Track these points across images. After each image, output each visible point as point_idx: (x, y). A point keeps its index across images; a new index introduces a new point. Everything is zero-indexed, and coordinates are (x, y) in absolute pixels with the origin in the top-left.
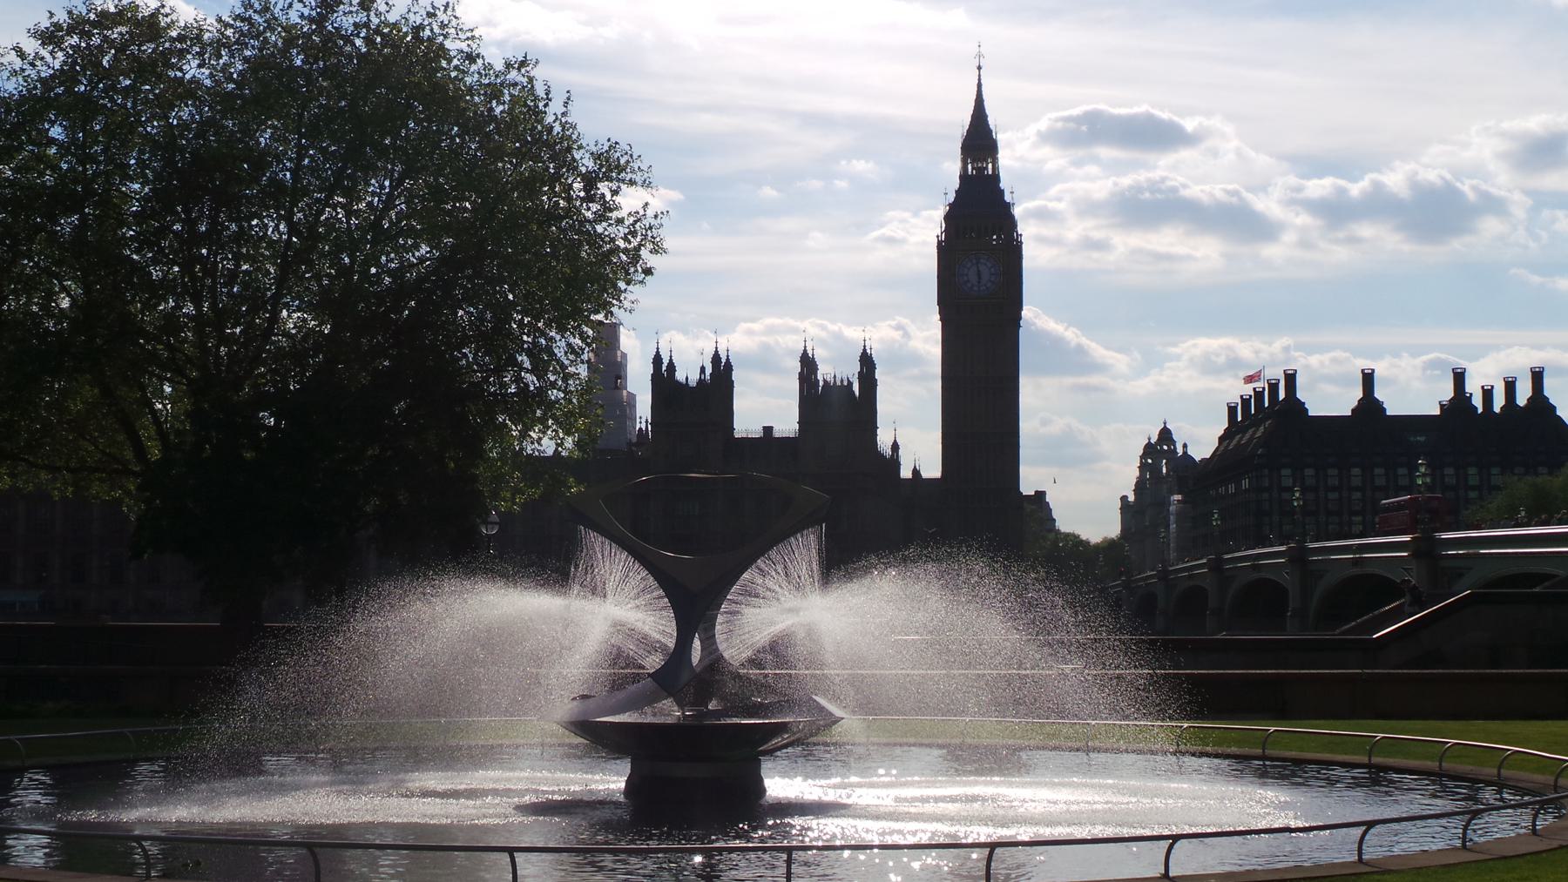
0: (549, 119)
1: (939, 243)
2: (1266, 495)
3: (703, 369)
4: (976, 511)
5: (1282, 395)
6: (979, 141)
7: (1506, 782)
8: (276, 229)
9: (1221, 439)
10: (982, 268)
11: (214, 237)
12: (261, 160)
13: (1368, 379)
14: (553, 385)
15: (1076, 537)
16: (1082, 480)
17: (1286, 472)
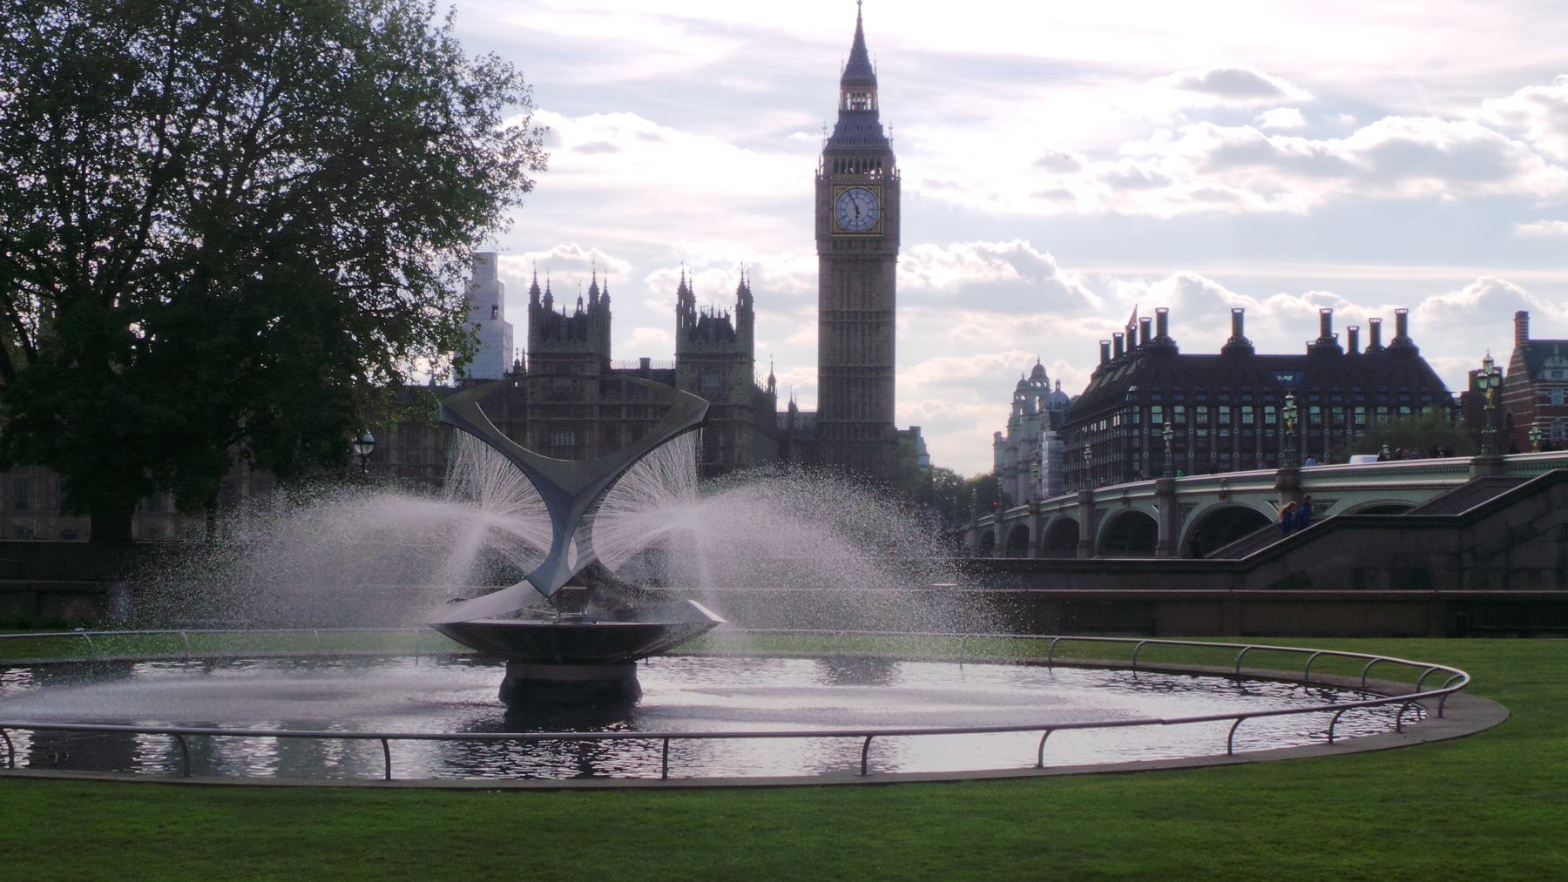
0: (429, 33)
1: (818, 177)
2: (1136, 433)
3: (580, 301)
4: (853, 434)
5: (1153, 334)
6: (859, 76)
7: (1370, 689)
8: (146, 142)
9: (1094, 377)
10: (858, 202)
11: (83, 147)
12: (133, 70)
14: (429, 302)
15: (950, 472)
16: (954, 404)
17: (1156, 409)
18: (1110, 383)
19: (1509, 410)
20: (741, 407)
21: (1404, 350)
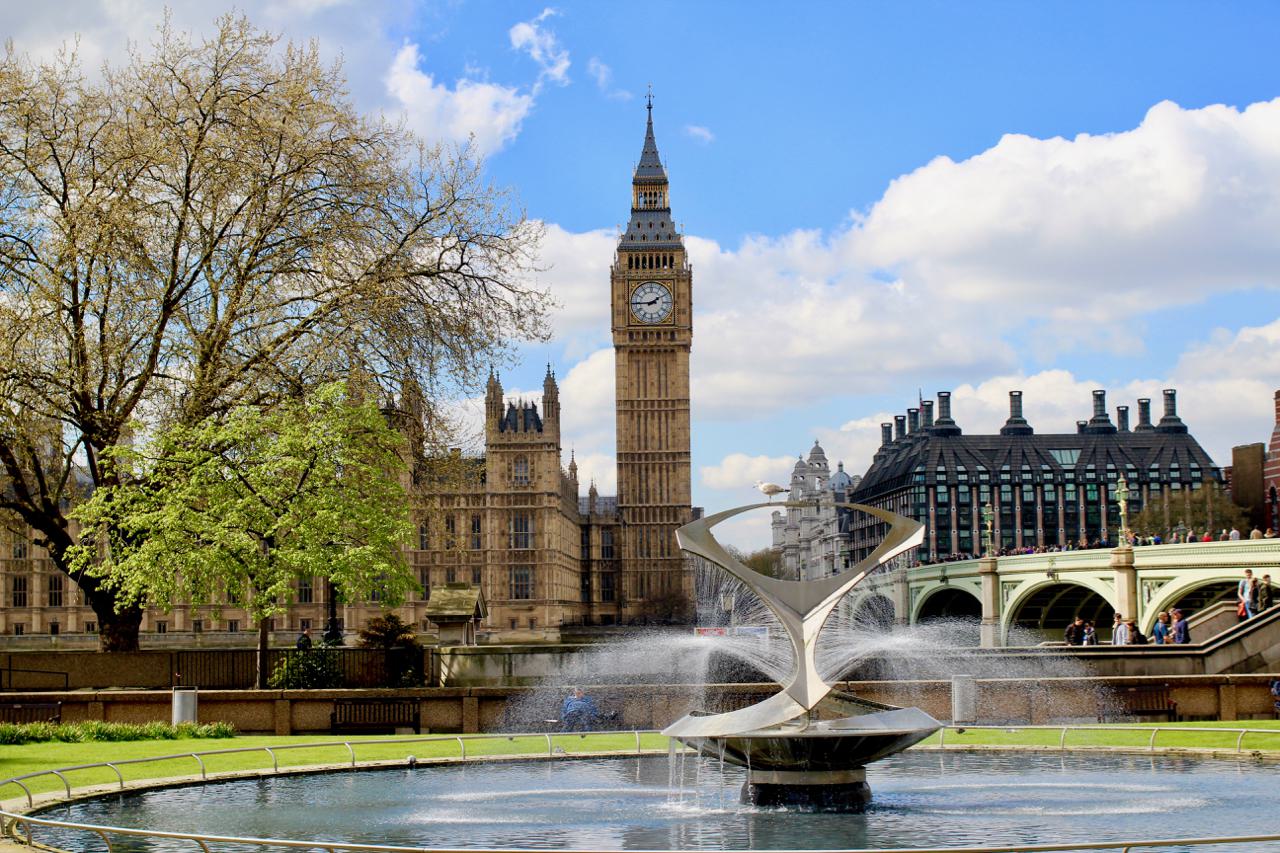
5: (936, 416)
9: (877, 458)
13: (1016, 399)
18: (895, 463)
19: (1272, 484)
20: (550, 494)
21: (1174, 429)
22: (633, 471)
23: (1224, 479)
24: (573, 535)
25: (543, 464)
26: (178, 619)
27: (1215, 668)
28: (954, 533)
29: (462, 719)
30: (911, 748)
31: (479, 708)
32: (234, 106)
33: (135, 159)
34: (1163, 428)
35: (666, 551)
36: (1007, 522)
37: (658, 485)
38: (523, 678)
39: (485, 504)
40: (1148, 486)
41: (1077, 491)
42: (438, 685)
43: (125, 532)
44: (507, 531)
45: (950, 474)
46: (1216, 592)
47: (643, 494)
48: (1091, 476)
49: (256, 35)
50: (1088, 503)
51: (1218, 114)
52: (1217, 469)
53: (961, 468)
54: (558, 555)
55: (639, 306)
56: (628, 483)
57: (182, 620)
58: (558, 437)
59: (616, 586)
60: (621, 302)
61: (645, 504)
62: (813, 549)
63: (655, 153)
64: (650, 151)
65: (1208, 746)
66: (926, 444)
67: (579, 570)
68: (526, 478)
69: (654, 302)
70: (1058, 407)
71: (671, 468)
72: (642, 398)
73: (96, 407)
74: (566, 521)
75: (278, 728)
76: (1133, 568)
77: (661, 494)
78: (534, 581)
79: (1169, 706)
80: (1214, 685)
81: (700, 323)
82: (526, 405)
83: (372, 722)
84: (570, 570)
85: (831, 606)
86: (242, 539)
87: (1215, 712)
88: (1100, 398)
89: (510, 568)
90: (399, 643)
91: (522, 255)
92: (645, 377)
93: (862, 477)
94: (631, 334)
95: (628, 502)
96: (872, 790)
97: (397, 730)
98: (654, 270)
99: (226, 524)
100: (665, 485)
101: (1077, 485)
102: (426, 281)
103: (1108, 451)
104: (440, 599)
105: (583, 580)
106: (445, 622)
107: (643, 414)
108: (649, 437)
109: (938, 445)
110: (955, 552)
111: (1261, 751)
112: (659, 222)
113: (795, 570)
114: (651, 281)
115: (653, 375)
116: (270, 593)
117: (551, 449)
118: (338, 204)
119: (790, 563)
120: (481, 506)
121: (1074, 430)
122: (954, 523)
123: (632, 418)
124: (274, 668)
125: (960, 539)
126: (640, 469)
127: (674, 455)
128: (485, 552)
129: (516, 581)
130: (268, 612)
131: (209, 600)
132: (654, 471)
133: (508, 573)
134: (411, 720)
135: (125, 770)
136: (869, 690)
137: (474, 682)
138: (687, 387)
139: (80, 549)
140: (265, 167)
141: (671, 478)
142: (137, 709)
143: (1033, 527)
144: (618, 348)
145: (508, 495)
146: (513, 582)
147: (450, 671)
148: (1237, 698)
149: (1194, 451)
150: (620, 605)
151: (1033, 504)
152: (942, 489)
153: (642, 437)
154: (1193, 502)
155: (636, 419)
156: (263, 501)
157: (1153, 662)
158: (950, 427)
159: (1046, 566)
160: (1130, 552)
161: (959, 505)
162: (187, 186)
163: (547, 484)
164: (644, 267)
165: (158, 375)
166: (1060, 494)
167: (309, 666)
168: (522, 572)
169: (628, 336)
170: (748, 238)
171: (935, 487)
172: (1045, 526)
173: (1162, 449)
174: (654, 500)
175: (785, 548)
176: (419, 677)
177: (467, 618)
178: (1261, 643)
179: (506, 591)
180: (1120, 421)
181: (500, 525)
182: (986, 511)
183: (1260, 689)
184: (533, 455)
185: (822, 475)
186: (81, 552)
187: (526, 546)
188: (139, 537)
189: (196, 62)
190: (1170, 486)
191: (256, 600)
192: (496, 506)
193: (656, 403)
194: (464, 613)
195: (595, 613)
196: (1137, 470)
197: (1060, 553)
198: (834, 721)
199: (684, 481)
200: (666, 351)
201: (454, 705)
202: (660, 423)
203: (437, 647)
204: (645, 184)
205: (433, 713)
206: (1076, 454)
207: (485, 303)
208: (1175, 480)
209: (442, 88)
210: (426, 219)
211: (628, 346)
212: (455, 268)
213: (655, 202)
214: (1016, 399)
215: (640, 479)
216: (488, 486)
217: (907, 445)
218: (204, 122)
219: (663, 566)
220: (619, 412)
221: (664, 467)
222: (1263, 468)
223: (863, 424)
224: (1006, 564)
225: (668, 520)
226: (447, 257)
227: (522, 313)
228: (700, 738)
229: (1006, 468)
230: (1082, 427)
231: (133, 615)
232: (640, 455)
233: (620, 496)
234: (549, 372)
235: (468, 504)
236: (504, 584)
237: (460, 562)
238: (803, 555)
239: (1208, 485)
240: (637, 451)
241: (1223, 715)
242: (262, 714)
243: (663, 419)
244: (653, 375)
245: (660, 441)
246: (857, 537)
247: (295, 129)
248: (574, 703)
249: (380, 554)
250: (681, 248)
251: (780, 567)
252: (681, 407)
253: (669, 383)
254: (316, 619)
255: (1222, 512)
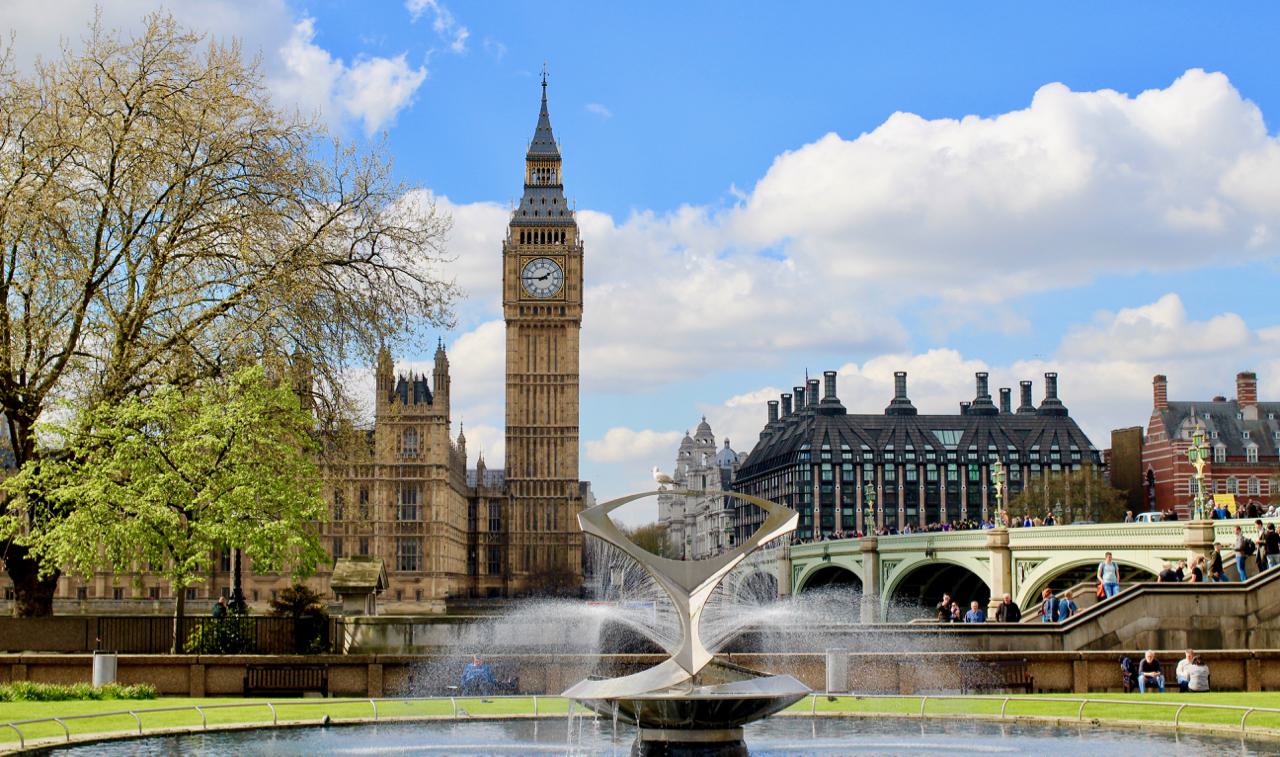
5: (822, 395)
9: (763, 435)
13: (901, 379)
18: (781, 441)
19: (1150, 467)
20: (439, 467)
21: (1055, 412)
22: (521, 445)
23: (1103, 461)
24: (460, 507)
25: (433, 436)
26: (99, 586)
27: (1074, 645)
28: (838, 512)
29: (366, 685)
30: (779, 713)
31: (384, 674)
32: (160, 100)
33: (62, 146)
34: (1044, 410)
35: (552, 525)
36: (890, 501)
37: (546, 459)
38: (423, 647)
39: (373, 475)
40: (1029, 467)
41: (959, 471)
42: (342, 653)
43: (52, 504)
44: (395, 503)
45: (834, 452)
46: (1088, 573)
47: (531, 468)
48: (973, 456)
49: (181, 33)
50: (970, 483)
51: (1109, 98)
52: (1097, 452)
53: (845, 447)
54: (445, 527)
55: (530, 281)
56: (515, 456)
57: (67, 587)
58: (448, 409)
59: (502, 559)
60: (513, 277)
61: (532, 478)
62: (698, 525)
63: (549, 130)
64: (544, 129)
65: (1054, 715)
66: (812, 422)
67: (466, 542)
68: (415, 450)
69: (545, 278)
70: (941, 386)
71: (559, 442)
72: (531, 372)
73: (18, 382)
74: (453, 493)
75: (192, 691)
76: (1008, 548)
77: (549, 467)
78: (421, 552)
79: (1026, 679)
80: (1070, 660)
81: (589, 295)
82: (416, 377)
83: (273, 686)
84: (457, 542)
85: (715, 583)
86: (162, 512)
87: (1069, 686)
88: (982, 379)
89: (397, 539)
90: (308, 612)
91: (430, 247)
92: (535, 352)
93: (749, 454)
94: (522, 308)
95: (516, 475)
96: (748, 748)
97: (305, 694)
98: (546, 246)
99: (149, 497)
100: (552, 459)
101: (959, 466)
102: (338, 270)
103: (990, 433)
104: (344, 571)
105: (469, 553)
106: (346, 593)
107: (532, 388)
108: (538, 411)
109: (824, 423)
110: (838, 531)
111: (1100, 719)
112: (552, 198)
113: (680, 545)
114: (543, 256)
115: (542, 349)
116: (189, 564)
117: (441, 421)
118: (253, 193)
119: (675, 538)
120: (370, 478)
121: (957, 411)
122: (838, 501)
123: (521, 392)
124: (190, 634)
125: (843, 516)
126: (528, 443)
127: (562, 430)
128: (373, 523)
129: (403, 552)
130: (187, 581)
131: (131, 568)
132: (542, 444)
133: (395, 544)
134: (320, 684)
135: (71, 725)
136: (750, 661)
137: (377, 650)
138: (576, 362)
139: (8, 519)
140: (188, 157)
141: (559, 453)
142: (59, 671)
143: (916, 506)
144: (509, 322)
145: (397, 467)
146: (400, 553)
147: (353, 640)
148: (1089, 672)
149: (1073, 433)
150: (506, 578)
151: (916, 483)
152: (827, 467)
153: (531, 411)
154: (1073, 484)
155: (525, 393)
156: (183, 477)
157: (1015, 639)
158: (835, 406)
159: (925, 545)
160: (1005, 533)
161: (844, 483)
162: (112, 174)
163: (436, 456)
164: (536, 243)
165: (76, 353)
166: (943, 474)
167: (224, 633)
168: (410, 544)
169: (518, 311)
170: (635, 213)
171: (820, 465)
172: (927, 506)
173: (1043, 431)
174: (542, 473)
175: (671, 523)
176: (326, 645)
177: (370, 589)
178: (1115, 623)
179: (393, 563)
180: (1002, 403)
181: (388, 497)
182: (869, 490)
183: (1110, 665)
184: (422, 428)
185: (709, 450)
186: (10, 522)
187: (414, 518)
188: (68, 508)
189: (124, 58)
190: (1050, 467)
191: (176, 570)
192: (384, 477)
193: (545, 378)
194: (367, 584)
195: (480, 586)
196: (1022, 449)
197: (947, 533)
198: (715, 686)
199: (571, 455)
200: (556, 326)
201: (360, 671)
202: (549, 397)
203: (340, 616)
204: (538, 161)
205: (338, 678)
206: (959, 435)
207: (394, 292)
208: (1055, 462)
209: (339, 64)
210: (341, 211)
211: (519, 320)
212: (366, 258)
213: (548, 178)
214: (901, 379)
215: (528, 453)
216: (377, 456)
217: (792, 423)
218: (130, 114)
219: (550, 539)
220: (508, 386)
221: (552, 441)
222: (1141, 451)
223: (746, 399)
224: (886, 543)
225: (555, 494)
226: (358, 248)
227: (430, 302)
228: (598, 699)
229: (890, 447)
230: (965, 408)
231: (51, 583)
232: (528, 429)
233: (508, 470)
234: (440, 345)
235: (356, 476)
236: (391, 555)
237: (347, 532)
238: (688, 530)
239: (1088, 468)
240: (525, 425)
241: (1076, 689)
242: (178, 677)
243: (552, 393)
244: (542, 349)
245: (549, 415)
246: (743, 513)
247: (213, 120)
248: (473, 670)
249: (292, 528)
250: (573, 225)
251: (665, 542)
252: (571, 382)
253: (559, 358)
254: (201, 587)
255: (1099, 494)
